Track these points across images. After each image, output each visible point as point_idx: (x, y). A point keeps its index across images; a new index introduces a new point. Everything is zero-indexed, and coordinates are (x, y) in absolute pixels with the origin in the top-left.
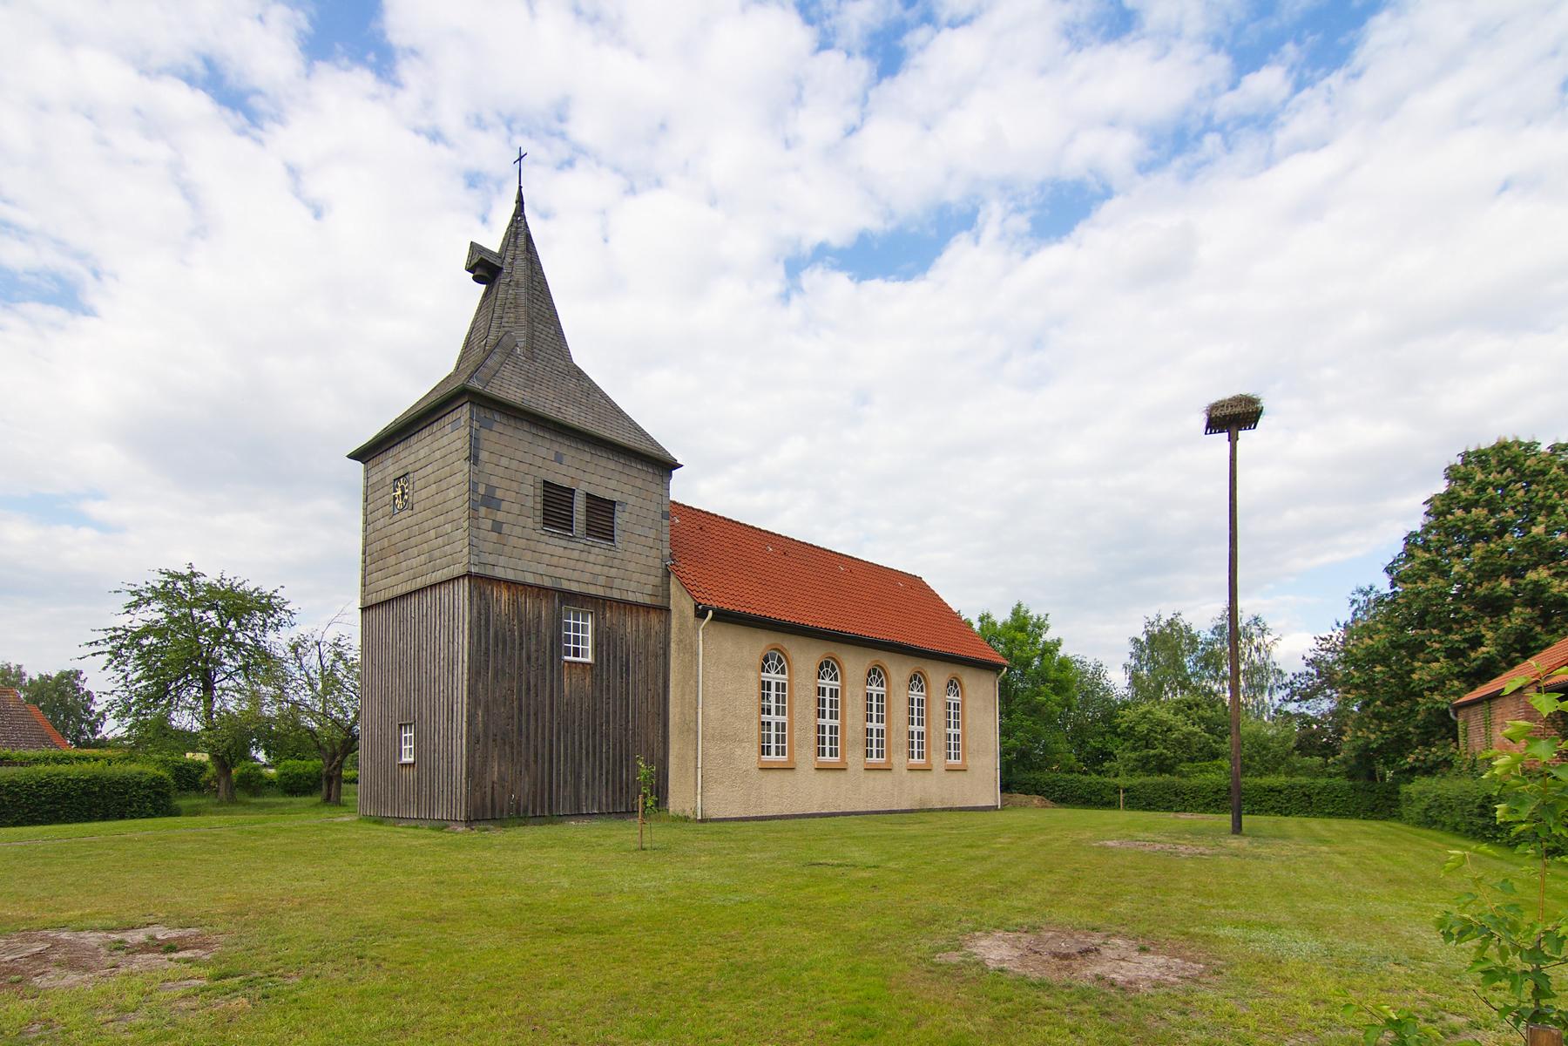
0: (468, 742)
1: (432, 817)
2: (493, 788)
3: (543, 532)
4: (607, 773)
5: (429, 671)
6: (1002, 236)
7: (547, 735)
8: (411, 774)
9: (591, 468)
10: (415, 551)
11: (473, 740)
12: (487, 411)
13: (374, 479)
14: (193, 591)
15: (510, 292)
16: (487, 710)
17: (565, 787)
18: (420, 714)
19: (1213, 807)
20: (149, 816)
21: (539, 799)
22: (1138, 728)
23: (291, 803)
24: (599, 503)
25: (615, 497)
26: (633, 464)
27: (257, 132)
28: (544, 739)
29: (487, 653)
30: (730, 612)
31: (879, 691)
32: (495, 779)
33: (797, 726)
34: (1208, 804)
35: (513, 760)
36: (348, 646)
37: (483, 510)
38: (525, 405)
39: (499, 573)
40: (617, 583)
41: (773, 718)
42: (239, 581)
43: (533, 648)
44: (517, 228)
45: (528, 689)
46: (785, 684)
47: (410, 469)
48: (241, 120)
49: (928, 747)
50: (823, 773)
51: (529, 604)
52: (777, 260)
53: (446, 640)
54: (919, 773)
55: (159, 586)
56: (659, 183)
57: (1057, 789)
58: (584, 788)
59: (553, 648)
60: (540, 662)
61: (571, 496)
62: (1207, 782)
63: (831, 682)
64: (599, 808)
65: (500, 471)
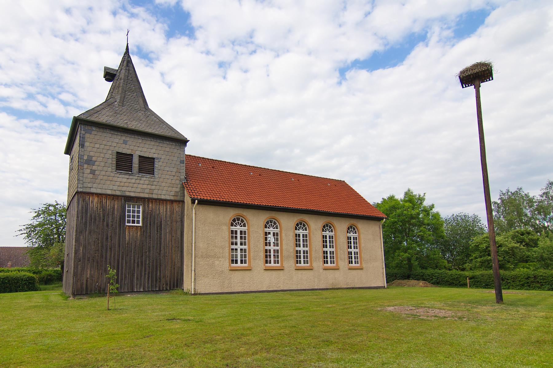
3: (116, 173)
4: (149, 273)
6: (440, 41)
7: (116, 257)
9: (142, 145)
12: (89, 126)
15: (118, 82)
16: (85, 247)
19: (526, 286)
20: (26, 291)
22: (481, 246)
24: (145, 159)
25: (155, 156)
27: (151, 65)
30: (208, 200)
31: (354, 235)
32: (88, 277)
34: (523, 285)
38: (108, 122)
39: (93, 190)
40: (155, 192)
41: (353, 250)
46: (357, 237)
48: (147, 61)
49: (337, 258)
50: (268, 272)
51: (108, 203)
52: (336, 70)
54: (331, 271)
55: (44, 209)
56: (288, 51)
57: (434, 277)
58: (135, 280)
59: (121, 221)
62: (521, 273)
63: (353, 234)
64: (144, 289)
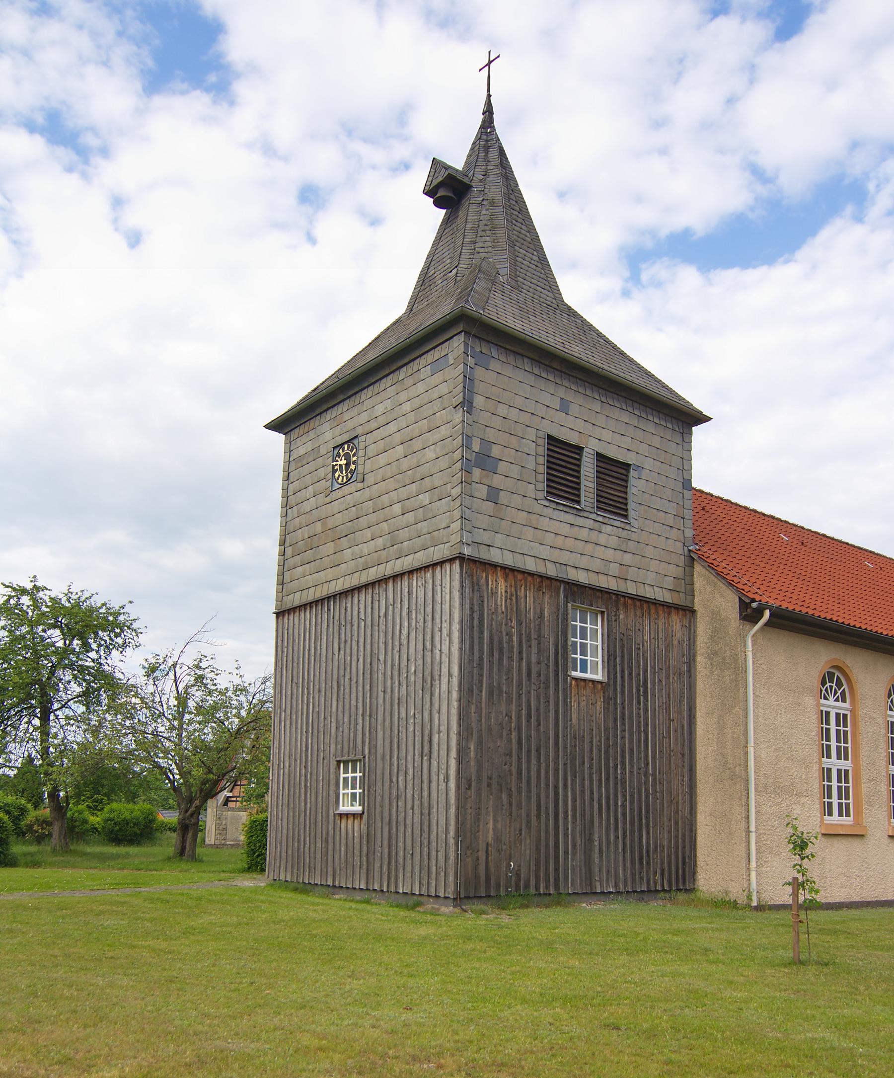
0: (458, 787)
1: (393, 889)
2: (487, 852)
3: (547, 503)
5: (389, 690)
8: (356, 828)
10: (368, 534)
11: (464, 783)
12: (483, 344)
13: (295, 455)
14: (36, 603)
15: (484, 212)
16: (480, 743)
17: (574, 854)
18: (373, 747)
21: (542, 868)
23: (127, 856)
25: (630, 459)
26: (650, 418)
28: (547, 785)
29: (480, 665)
32: (490, 840)
33: (865, 775)
35: (511, 814)
36: (210, 669)
37: (477, 473)
39: (495, 556)
40: (632, 573)
42: (87, 595)
43: (534, 658)
44: (487, 141)
45: (529, 716)
46: (847, 715)
47: (360, 430)
48: (73, 156)
51: (529, 598)
53: (420, 646)
60: (542, 678)
61: (578, 457)
65: (497, 422)
